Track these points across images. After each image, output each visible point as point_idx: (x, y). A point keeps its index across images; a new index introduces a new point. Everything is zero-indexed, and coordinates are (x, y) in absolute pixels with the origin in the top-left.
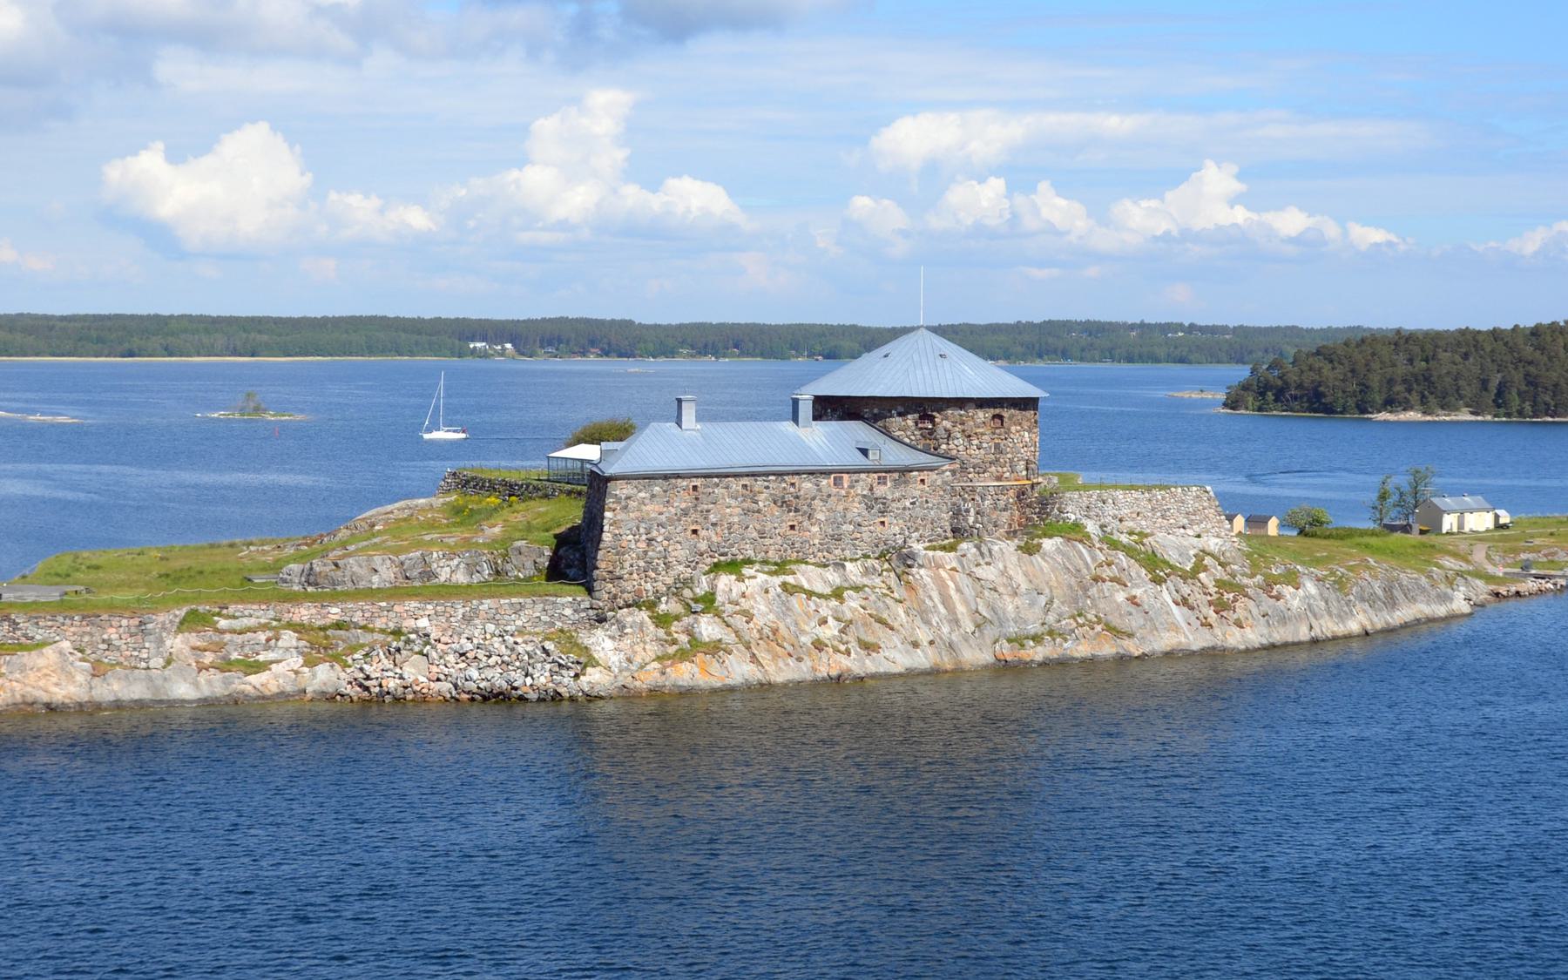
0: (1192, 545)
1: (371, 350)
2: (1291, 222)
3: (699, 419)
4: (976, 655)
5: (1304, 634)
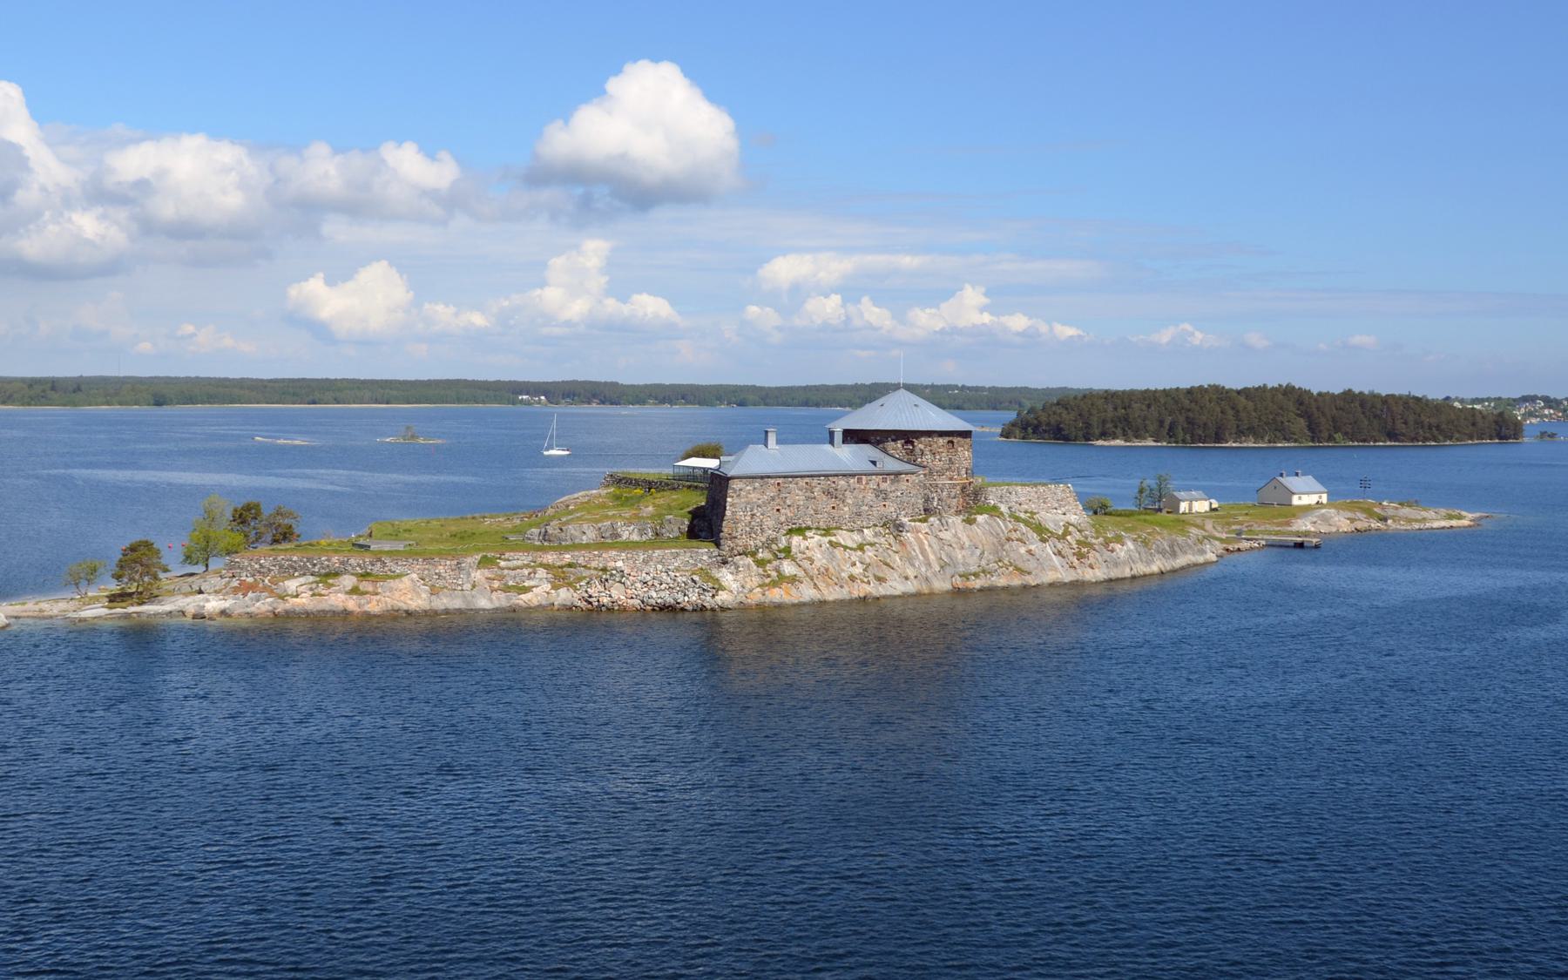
0: (1062, 520)
1: (459, 401)
2: (1018, 322)
3: (779, 442)
4: (942, 585)
5: (1127, 573)
